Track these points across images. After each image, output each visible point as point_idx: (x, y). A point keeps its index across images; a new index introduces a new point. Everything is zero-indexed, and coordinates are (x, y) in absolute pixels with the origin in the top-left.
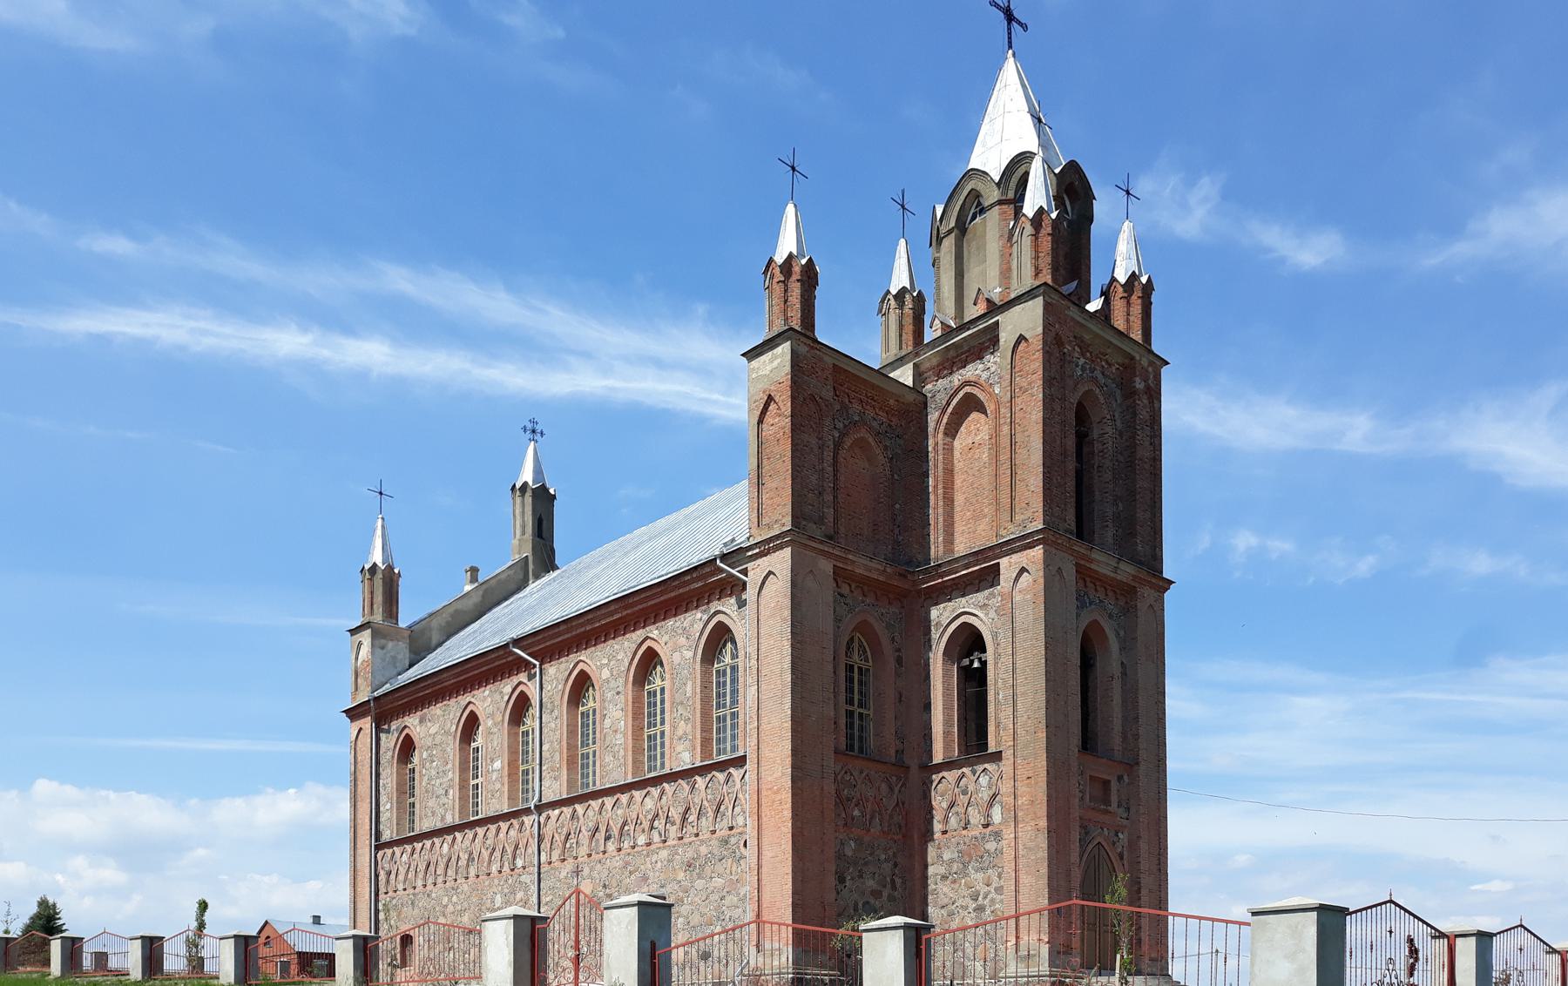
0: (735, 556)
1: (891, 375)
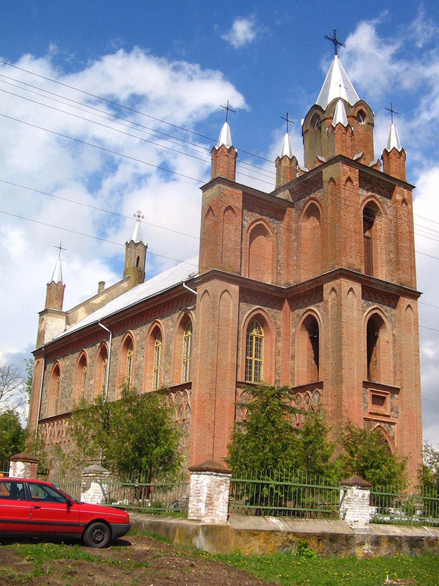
0: (191, 282)
1: (278, 196)
